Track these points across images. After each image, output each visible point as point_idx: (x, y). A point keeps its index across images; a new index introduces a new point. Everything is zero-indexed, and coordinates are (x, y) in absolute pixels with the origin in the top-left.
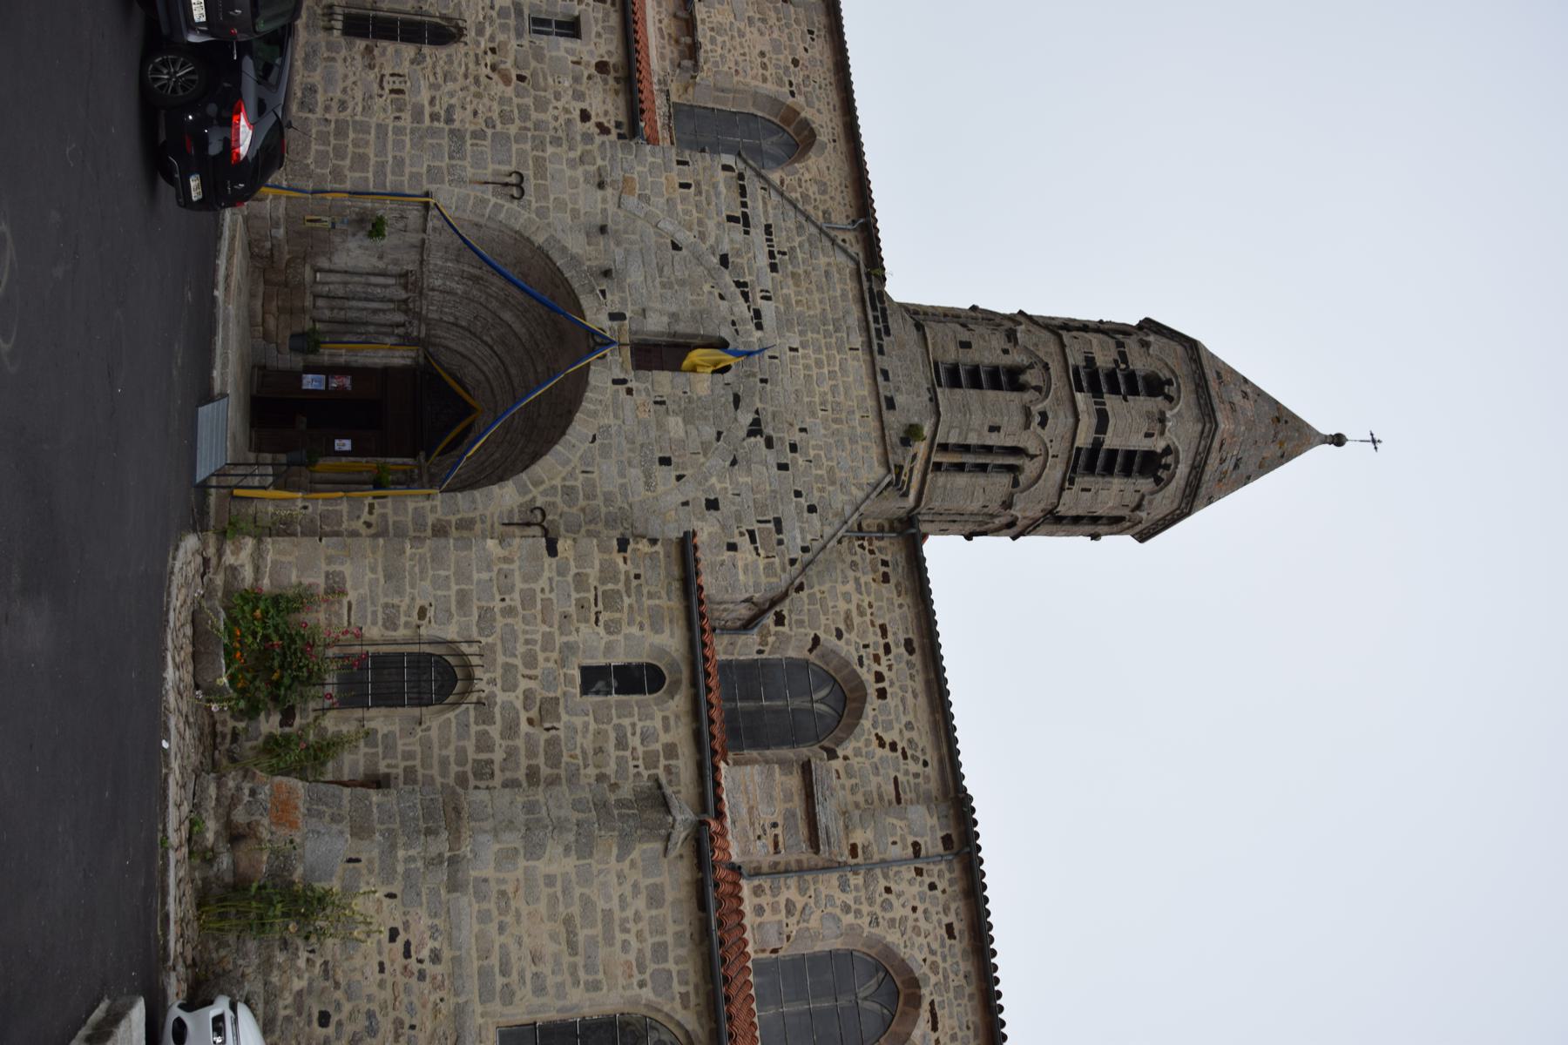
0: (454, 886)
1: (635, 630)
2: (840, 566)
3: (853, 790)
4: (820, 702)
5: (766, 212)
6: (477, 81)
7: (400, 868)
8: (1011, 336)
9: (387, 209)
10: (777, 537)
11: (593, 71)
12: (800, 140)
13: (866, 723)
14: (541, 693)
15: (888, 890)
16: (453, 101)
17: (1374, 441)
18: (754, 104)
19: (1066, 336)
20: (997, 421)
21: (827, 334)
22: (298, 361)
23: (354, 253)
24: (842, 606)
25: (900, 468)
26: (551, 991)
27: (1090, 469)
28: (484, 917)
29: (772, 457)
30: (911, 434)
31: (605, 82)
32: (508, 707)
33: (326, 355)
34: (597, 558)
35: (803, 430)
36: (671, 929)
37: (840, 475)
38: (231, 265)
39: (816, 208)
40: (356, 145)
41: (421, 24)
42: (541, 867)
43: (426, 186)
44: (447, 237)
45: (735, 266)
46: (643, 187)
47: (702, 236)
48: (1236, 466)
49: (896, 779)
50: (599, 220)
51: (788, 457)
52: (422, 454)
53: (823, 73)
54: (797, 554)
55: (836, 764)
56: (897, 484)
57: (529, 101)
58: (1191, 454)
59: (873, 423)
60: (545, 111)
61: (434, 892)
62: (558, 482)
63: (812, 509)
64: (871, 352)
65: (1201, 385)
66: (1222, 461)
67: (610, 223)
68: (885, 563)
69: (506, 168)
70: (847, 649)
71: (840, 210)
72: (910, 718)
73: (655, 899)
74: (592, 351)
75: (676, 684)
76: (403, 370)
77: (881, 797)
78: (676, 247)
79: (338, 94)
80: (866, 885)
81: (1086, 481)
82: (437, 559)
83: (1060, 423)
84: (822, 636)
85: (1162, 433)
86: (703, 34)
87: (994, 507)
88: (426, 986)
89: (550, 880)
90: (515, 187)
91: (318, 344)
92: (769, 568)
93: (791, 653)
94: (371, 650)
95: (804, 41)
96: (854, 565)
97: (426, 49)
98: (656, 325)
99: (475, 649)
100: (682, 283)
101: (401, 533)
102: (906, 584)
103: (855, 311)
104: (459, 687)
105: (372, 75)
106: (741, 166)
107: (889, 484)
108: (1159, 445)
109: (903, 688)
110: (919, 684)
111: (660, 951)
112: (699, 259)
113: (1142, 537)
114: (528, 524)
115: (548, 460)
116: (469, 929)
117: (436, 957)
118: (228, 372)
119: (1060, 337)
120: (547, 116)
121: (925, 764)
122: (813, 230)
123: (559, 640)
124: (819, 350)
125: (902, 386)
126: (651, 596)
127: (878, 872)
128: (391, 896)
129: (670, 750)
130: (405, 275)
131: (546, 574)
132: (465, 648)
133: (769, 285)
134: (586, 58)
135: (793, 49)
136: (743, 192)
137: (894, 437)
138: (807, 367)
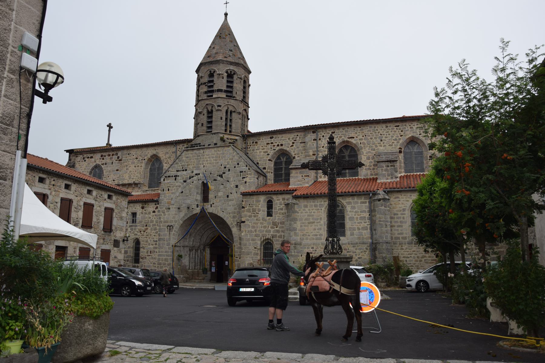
0: (300, 244)
1: (260, 206)
2: (253, 154)
3: (302, 153)
4: (284, 159)
5: (174, 171)
6: (148, 235)
7: (296, 254)
8: (200, 113)
9: (176, 254)
10: (244, 172)
11: (144, 210)
12: (155, 159)
13: (288, 149)
14: (271, 225)
15: (323, 147)
16: (152, 240)
17: (226, 3)
18: (147, 169)
19: (200, 99)
20: (220, 118)
21: (201, 158)
22: (209, 273)
23: (186, 261)
24: (262, 153)
25: (230, 143)
26: (321, 227)
27: (231, 92)
28: (307, 239)
29: (227, 173)
30: (222, 139)
31: (146, 207)
32: (274, 232)
33: (208, 267)
34: (245, 213)
35: (221, 165)
36: (312, 204)
37: (231, 157)
38: (188, 285)
39: (172, 155)
40: (163, 261)
41: (135, 247)
42: (299, 228)
43: (171, 246)
44: (181, 241)
45: (186, 179)
46: (169, 199)
47: (180, 186)
48: (231, 51)
49: (300, 143)
50: (177, 209)
51: (227, 169)
52: (228, 246)
53: (139, 152)
54: (247, 168)
55: (296, 156)
56: (233, 143)
57: (151, 224)
58: (228, 65)
59: (220, 149)
60: (153, 221)
61: (301, 248)
62: (232, 219)
63: (238, 164)
64: (204, 148)
65: (211, 63)
66: (230, 56)
67: (178, 207)
68: (253, 143)
69: (166, 229)
70: (271, 153)
71: (172, 149)
72: (287, 138)
73: (306, 206)
74: (205, 211)
75: (271, 197)
76: (210, 250)
77: (304, 147)
78: (182, 192)
79: (152, 264)
80: (322, 152)
81: (234, 93)
82: (245, 245)
83: (220, 102)
84: (269, 159)
85: (222, 74)
86: (131, 181)
87: (240, 116)
88: (317, 250)
89: (301, 226)
90: (170, 227)
91: (205, 268)
92: (250, 174)
93: (273, 165)
94: (262, 258)
95: (131, 156)
96: (253, 150)
97: (141, 246)
98: (199, 197)
99: (262, 238)
100: (190, 191)
101: (240, 252)
102: (258, 138)
103: (195, 151)
104: (270, 241)
105: (148, 257)
106: (163, 177)
107: (233, 146)
108: (226, 74)
109: (281, 140)
110: (280, 136)
111: (316, 206)
112: (185, 187)
113: (249, 72)
114: (240, 226)
115: (227, 221)
116: (309, 242)
117: (313, 248)
118: (210, 286)
119: (200, 100)
120: (155, 220)
121: (297, 135)
122: (177, 160)
123: (261, 221)
124: (204, 160)
125: (212, 141)
126: (253, 202)
127: (319, 149)
128: (301, 256)
129: (284, 199)
130: (190, 250)
131: (249, 223)
132: (262, 240)
133: (190, 171)
134: (141, 211)
135: (133, 159)
136: (169, 176)
137: (223, 144)
138: (208, 163)
